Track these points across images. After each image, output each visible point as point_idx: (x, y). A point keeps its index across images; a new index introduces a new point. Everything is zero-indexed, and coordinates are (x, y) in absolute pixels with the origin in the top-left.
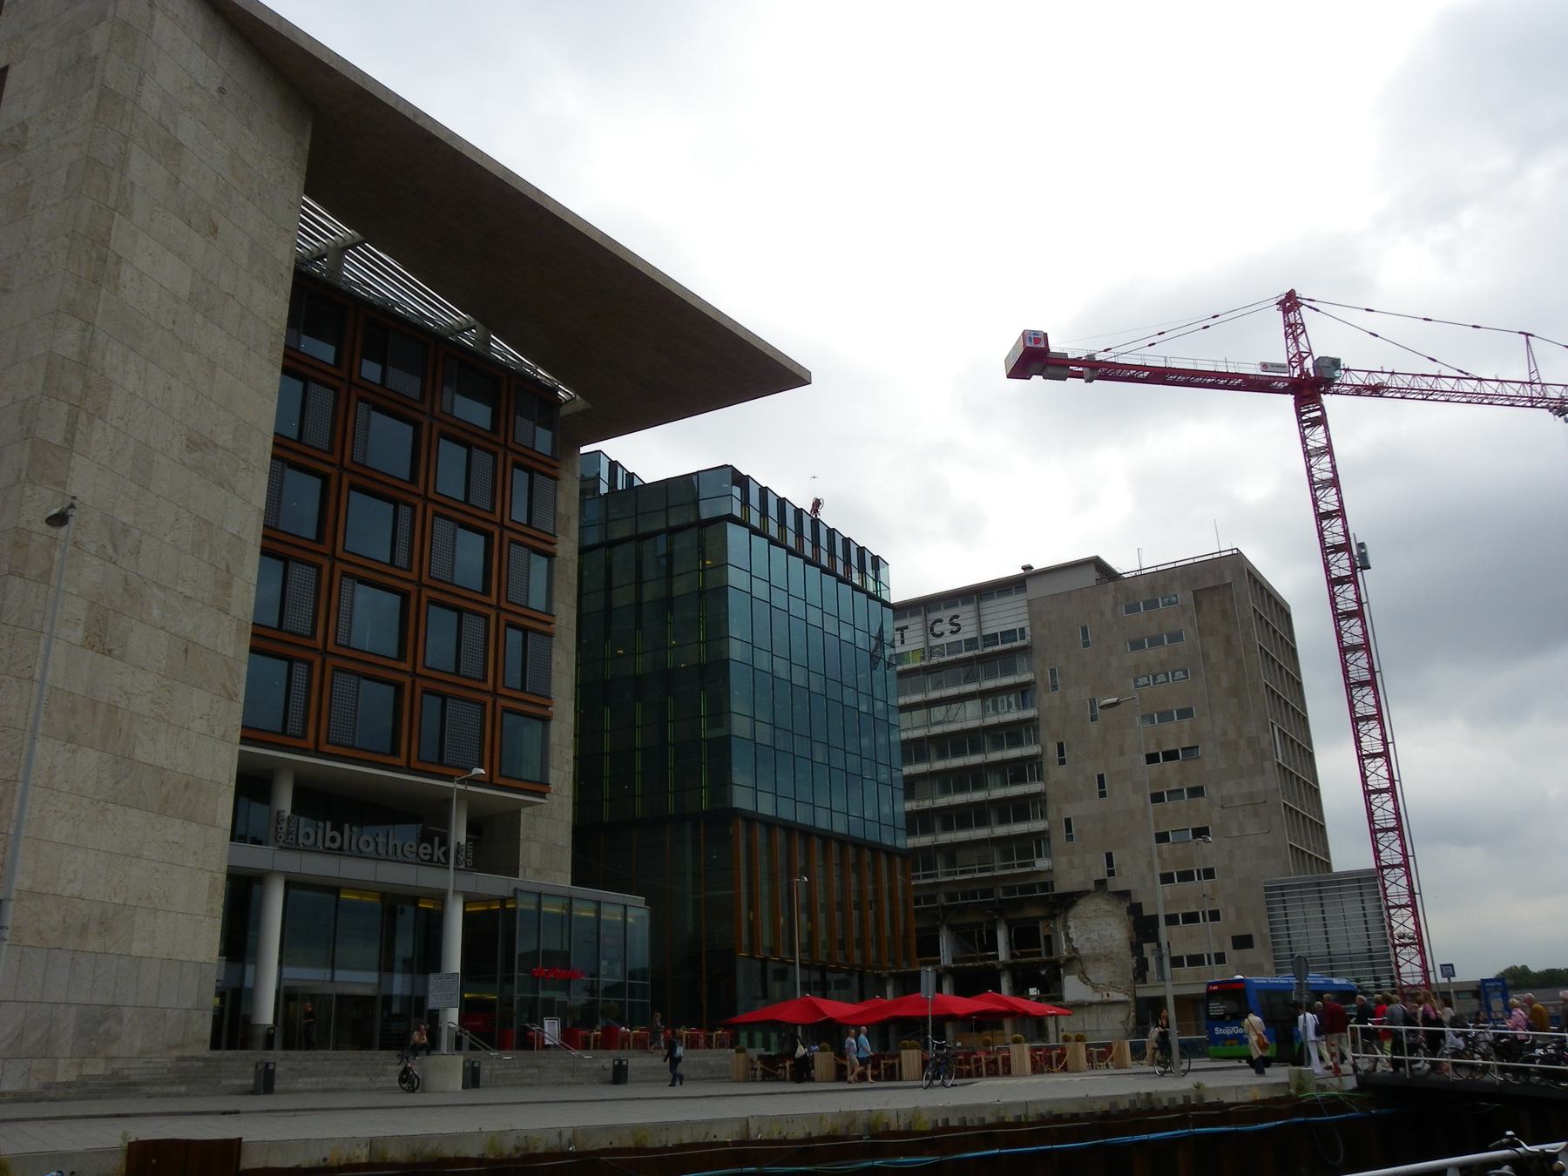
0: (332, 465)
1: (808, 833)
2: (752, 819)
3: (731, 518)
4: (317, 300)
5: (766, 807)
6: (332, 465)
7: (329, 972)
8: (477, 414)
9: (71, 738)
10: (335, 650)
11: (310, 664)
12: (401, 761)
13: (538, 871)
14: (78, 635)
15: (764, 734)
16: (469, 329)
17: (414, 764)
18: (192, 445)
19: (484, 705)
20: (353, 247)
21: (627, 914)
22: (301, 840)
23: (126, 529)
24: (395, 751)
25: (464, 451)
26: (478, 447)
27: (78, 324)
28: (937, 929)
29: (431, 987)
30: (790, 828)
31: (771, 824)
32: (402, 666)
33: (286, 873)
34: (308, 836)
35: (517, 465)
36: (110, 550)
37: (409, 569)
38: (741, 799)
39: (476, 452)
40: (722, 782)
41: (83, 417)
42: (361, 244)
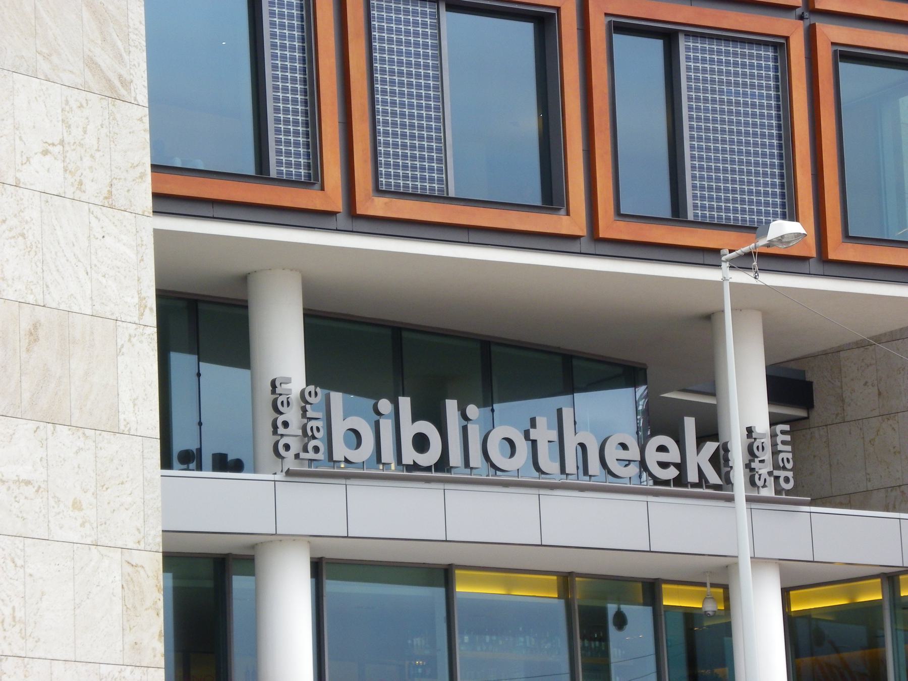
12: (573, 222)
17: (609, 227)
24: (552, 197)
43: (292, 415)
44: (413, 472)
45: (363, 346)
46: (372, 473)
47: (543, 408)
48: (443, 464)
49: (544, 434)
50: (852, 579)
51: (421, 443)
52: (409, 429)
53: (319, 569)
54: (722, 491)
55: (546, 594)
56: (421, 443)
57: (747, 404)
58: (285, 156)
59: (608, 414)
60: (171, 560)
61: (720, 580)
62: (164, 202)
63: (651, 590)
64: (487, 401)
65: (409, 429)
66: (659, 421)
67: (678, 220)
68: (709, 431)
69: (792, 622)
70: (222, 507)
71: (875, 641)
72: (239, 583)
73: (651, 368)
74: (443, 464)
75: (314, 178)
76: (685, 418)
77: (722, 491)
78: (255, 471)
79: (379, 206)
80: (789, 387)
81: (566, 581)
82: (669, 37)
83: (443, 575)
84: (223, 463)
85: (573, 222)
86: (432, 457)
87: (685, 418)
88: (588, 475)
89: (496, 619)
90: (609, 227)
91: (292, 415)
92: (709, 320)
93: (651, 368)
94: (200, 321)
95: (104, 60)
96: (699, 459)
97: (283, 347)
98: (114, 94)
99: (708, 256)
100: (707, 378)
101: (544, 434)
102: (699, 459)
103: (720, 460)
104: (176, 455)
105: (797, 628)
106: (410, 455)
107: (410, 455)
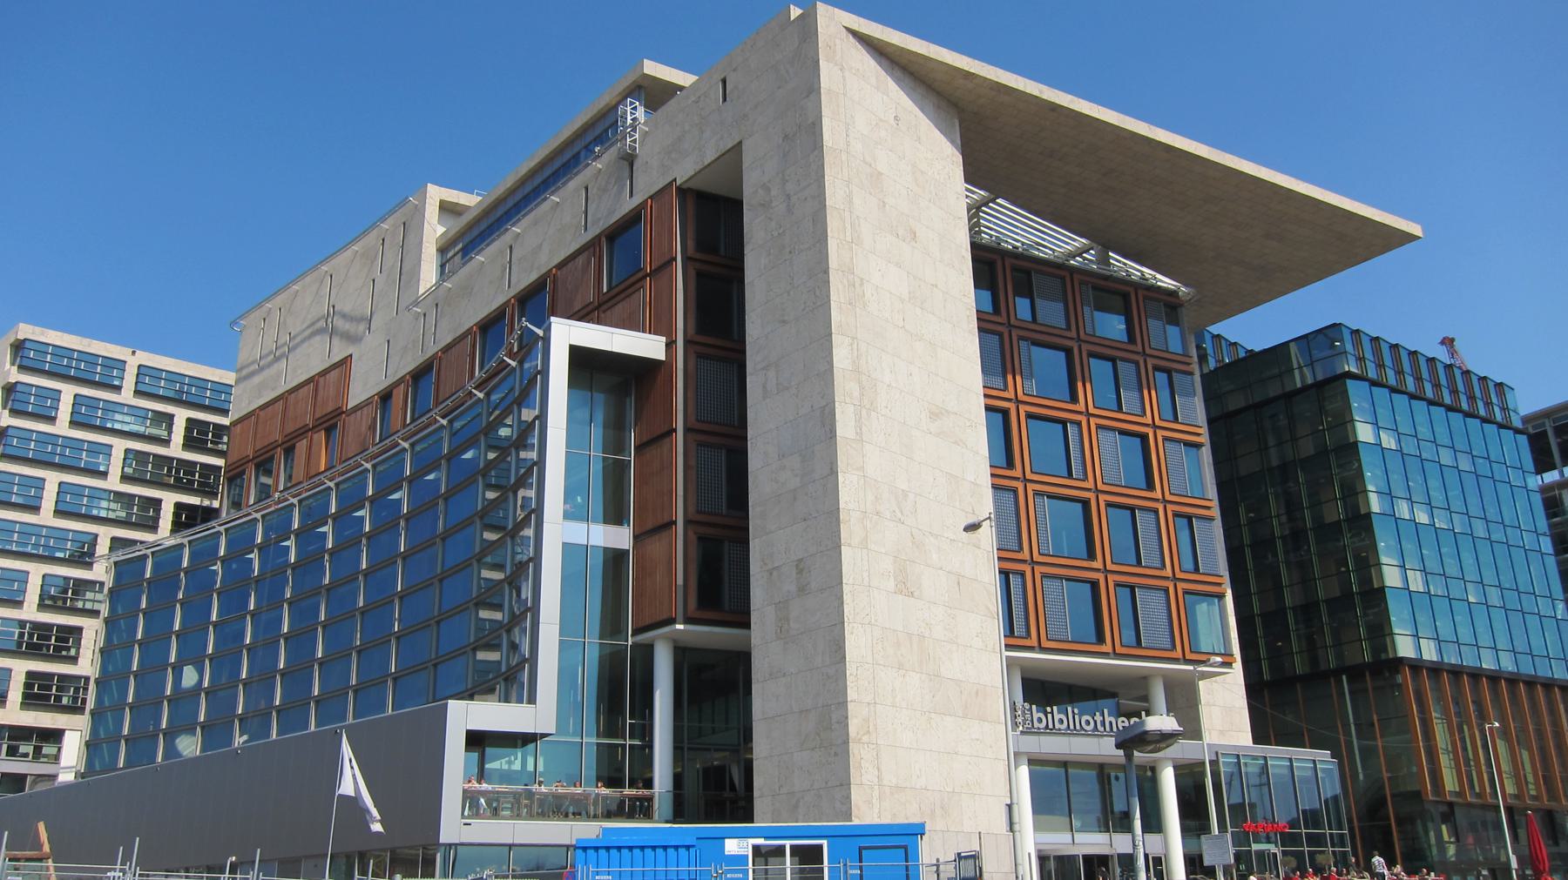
0: (1009, 400)
1: (1476, 675)
2: (1416, 666)
3: (1349, 375)
4: (992, 266)
5: (1429, 653)
6: (1009, 400)
7: (1069, 836)
8: (1112, 326)
9: (900, 667)
10: (1041, 559)
11: (1023, 574)
12: (1034, 642)
13: (1222, 732)
14: (891, 584)
15: (1416, 582)
16: (1087, 251)
17: (1119, 650)
18: (935, 415)
19: (1166, 590)
20: (986, 205)
21: (1310, 767)
22: (1036, 724)
23: (905, 494)
24: (1100, 639)
25: (1109, 364)
26: (1123, 359)
27: (847, 341)
28: (476, 662)
29: (1204, 847)
30: (1456, 672)
31: (1435, 670)
32: (1095, 565)
33: (1173, 759)
34: (1040, 720)
35: (1156, 368)
37: (1085, 479)
38: (1405, 647)
39: (1119, 363)
40: (1381, 631)
41: (864, 412)
42: (993, 201)
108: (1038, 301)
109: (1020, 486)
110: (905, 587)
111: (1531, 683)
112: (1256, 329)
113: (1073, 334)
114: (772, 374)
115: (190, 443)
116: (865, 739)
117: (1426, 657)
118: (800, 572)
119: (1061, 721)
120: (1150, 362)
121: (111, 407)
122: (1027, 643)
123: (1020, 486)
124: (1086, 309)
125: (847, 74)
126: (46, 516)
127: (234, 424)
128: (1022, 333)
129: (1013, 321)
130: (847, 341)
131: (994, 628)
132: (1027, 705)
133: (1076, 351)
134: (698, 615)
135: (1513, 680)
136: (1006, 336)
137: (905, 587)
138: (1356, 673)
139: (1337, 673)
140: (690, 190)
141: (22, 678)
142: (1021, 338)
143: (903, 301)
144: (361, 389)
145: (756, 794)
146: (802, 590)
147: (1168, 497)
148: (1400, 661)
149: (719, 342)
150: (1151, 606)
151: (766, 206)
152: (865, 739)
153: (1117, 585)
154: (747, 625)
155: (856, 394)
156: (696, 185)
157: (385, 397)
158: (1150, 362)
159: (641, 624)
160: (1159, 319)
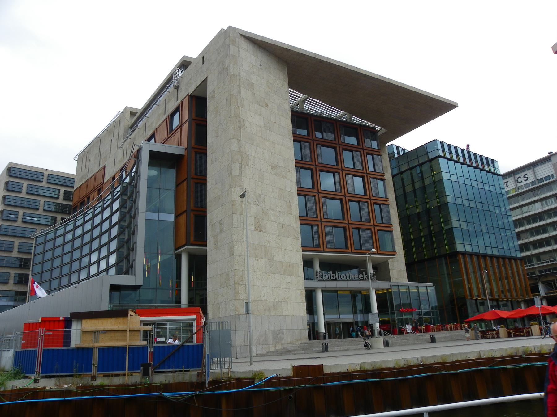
1: (485, 256)
2: (464, 254)
3: (440, 157)
4: (300, 119)
5: (468, 249)
8: (352, 141)
9: (256, 257)
11: (318, 225)
12: (349, 250)
13: (397, 279)
17: (353, 251)
18: (273, 168)
19: (371, 230)
20: (306, 100)
21: (427, 289)
23: (260, 195)
24: (347, 247)
27: (237, 141)
30: (478, 255)
31: (471, 255)
35: (368, 154)
36: (257, 202)
38: (460, 248)
39: (354, 152)
40: (452, 243)
41: (243, 166)
42: (308, 98)
43: (318, 274)
44: (332, 280)
45: (327, 266)
46: (327, 280)
47: (347, 272)
48: (336, 279)
49: (347, 275)
50: (383, 289)
51: (333, 277)
52: (332, 275)
53: (322, 291)
54: (368, 280)
55: (348, 293)
56: (333, 277)
57: (370, 270)
58: (316, 245)
59: (355, 272)
60: (306, 291)
61: (368, 290)
62: (303, 251)
63: (360, 292)
64: (340, 271)
65: (332, 275)
66: (360, 272)
67: (361, 249)
68: (366, 273)
69: (376, 294)
70: (312, 284)
71: (386, 296)
72: (313, 293)
73: (360, 266)
74: (336, 279)
75: (320, 247)
76: (75, 173)
77: (368, 280)
78: (532, 336)
79: (327, 250)
80: (375, 268)
81: (351, 291)
82: (359, 229)
83: (336, 291)
84: (311, 280)
85: (349, 250)
86: (334, 278)
87: (75, 173)
88: (352, 280)
89: (342, 296)
90: (353, 251)
91: (318, 274)
92: (365, 261)
93: (360, 266)
94: (307, 263)
95: (296, 235)
96: (365, 277)
97: (317, 267)
98: (297, 239)
99: (365, 254)
100: (366, 267)
101: (347, 275)
102: (365, 277)
103: (368, 277)
104: (306, 279)
105: (377, 296)
106: (332, 278)
107: (332, 278)
108: (324, 133)
109: (316, 195)
110: (259, 228)
111: (504, 258)
112: (409, 141)
113: (337, 142)
114: (214, 155)
115: (65, 199)
116: (241, 283)
117: (494, 253)
118: (221, 224)
119: (326, 276)
120: (365, 151)
121: (40, 188)
122: (319, 249)
123: (316, 195)
124: (342, 136)
125: (240, 50)
126: (19, 223)
127: (75, 191)
128: (317, 142)
129: (314, 138)
130: (237, 141)
131: (298, 244)
132: (321, 271)
133: (338, 148)
134: (194, 243)
135: (498, 257)
136: (312, 143)
137: (259, 228)
138: (445, 256)
139: (440, 257)
140: (194, 96)
141: (13, 275)
142: (317, 144)
143: (261, 127)
144: (108, 177)
145: (208, 304)
146: (221, 230)
147: (372, 198)
148: (458, 252)
149: (200, 147)
150: (365, 234)
151: (213, 97)
152: (241, 283)
153: (353, 228)
154: (206, 246)
155: (240, 160)
156: (195, 94)
157: (114, 178)
158: (365, 151)
159: (177, 247)
160: (369, 139)
